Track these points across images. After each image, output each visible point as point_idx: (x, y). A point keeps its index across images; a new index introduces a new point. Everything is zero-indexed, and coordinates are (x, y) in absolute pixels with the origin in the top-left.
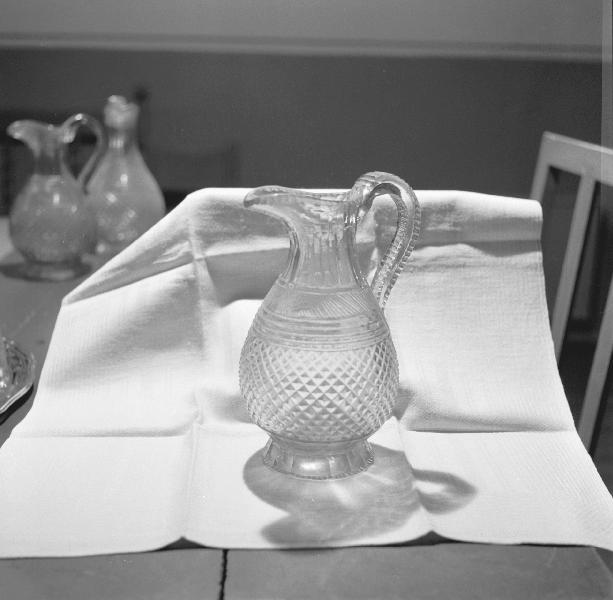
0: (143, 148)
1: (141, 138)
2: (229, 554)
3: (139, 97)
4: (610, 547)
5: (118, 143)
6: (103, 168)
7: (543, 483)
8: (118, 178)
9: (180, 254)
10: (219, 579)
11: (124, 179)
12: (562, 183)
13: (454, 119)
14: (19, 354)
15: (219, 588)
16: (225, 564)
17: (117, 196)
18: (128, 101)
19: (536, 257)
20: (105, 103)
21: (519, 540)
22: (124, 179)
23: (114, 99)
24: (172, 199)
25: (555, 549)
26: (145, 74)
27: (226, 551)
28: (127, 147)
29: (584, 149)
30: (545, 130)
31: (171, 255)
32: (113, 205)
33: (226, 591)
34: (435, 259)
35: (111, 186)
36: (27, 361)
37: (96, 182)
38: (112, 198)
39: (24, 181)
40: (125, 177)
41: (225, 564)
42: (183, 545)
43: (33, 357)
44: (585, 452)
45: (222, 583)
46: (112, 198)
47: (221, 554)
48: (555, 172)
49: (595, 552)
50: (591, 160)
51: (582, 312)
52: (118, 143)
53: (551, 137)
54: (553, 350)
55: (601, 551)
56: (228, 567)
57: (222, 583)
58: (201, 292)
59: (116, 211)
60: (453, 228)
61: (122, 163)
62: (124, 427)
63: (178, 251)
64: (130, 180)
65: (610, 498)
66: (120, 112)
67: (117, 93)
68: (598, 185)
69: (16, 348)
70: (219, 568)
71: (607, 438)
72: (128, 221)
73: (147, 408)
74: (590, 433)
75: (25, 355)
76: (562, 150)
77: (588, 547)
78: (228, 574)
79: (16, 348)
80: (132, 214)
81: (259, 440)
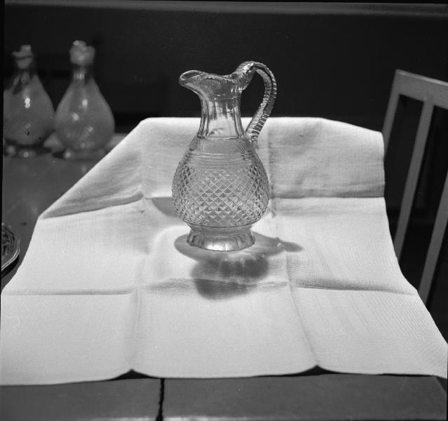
1: (96, 72)
2: (166, 382)
3: (92, 42)
5: (80, 76)
6: (69, 95)
9: (135, 193)
10: (158, 400)
11: (85, 103)
12: (410, 107)
14: (9, 233)
18: (88, 45)
19: (380, 203)
21: (381, 372)
22: (85, 103)
23: (77, 43)
24: (125, 123)
25: (406, 378)
27: (163, 380)
29: (425, 82)
31: (126, 194)
32: (77, 122)
33: (164, 408)
34: (312, 208)
35: (75, 107)
36: (14, 239)
38: (76, 117)
40: (86, 103)
42: (132, 375)
43: (19, 242)
45: (161, 403)
46: (76, 117)
47: (159, 381)
48: (403, 99)
50: (430, 91)
52: (80, 76)
53: (401, 74)
54: (394, 253)
55: (439, 379)
56: (165, 391)
57: (161, 403)
60: (323, 189)
61: (84, 91)
62: (86, 288)
63: (134, 191)
64: (89, 104)
66: (81, 53)
67: (79, 40)
70: (158, 392)
73: (105, 266)
76: (409, 83)
78: (165, 396)
81: (185, 229)
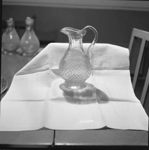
0: (35, 30)
1: (34, 27)
2: (56, 131)
3: (34, 17)
4: (148, 130)
5: (29, 29)
7: (126, 112)
8: (29, 37)
10: (53, 137)
11: (30, 37)
12: (138, 40)
13: (108, 27)
14: (4, 81)
15: (53, 139)
16: (55, 133)
17: (28, 41)
18: (31, 18)
20: (26, 19)
21: (127, 129)
22: (30, 37)
23: (28, 18)
24: (43, 44)
26: (35, 12)
27: (55, 130)
28: (31, 29)
30: (133, 28)
32: (27, 44)
35: (27, 39)
36: (6, 82)
37: (23, 38)
38: (27, 42)
39: (3, 33)
40: (30, 38)
41: (55, 133)
44: (142, 107)
46: (27, 42)
47: (53, 131)
48: (136, 38)
49: (146, 132)
51: (141, 73)
53: (135, 29)
55: (147, 131)
58: (64, 99)
59: (28, 45)
61: (30, 33)
64: (32, 38)
65: (147, 118)
66: (29, 21)
67: (29, 16)
68: (146, 41)
69: (3, 79)
71: (147, 102)
72: (31, 48)
73: (37, 94)
74: (143, 103)
75: (5, 81)
77: (144, 131)
79: (3, 79)
80: (32, 46)
